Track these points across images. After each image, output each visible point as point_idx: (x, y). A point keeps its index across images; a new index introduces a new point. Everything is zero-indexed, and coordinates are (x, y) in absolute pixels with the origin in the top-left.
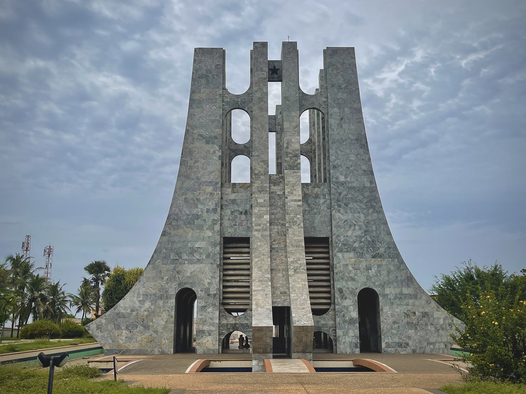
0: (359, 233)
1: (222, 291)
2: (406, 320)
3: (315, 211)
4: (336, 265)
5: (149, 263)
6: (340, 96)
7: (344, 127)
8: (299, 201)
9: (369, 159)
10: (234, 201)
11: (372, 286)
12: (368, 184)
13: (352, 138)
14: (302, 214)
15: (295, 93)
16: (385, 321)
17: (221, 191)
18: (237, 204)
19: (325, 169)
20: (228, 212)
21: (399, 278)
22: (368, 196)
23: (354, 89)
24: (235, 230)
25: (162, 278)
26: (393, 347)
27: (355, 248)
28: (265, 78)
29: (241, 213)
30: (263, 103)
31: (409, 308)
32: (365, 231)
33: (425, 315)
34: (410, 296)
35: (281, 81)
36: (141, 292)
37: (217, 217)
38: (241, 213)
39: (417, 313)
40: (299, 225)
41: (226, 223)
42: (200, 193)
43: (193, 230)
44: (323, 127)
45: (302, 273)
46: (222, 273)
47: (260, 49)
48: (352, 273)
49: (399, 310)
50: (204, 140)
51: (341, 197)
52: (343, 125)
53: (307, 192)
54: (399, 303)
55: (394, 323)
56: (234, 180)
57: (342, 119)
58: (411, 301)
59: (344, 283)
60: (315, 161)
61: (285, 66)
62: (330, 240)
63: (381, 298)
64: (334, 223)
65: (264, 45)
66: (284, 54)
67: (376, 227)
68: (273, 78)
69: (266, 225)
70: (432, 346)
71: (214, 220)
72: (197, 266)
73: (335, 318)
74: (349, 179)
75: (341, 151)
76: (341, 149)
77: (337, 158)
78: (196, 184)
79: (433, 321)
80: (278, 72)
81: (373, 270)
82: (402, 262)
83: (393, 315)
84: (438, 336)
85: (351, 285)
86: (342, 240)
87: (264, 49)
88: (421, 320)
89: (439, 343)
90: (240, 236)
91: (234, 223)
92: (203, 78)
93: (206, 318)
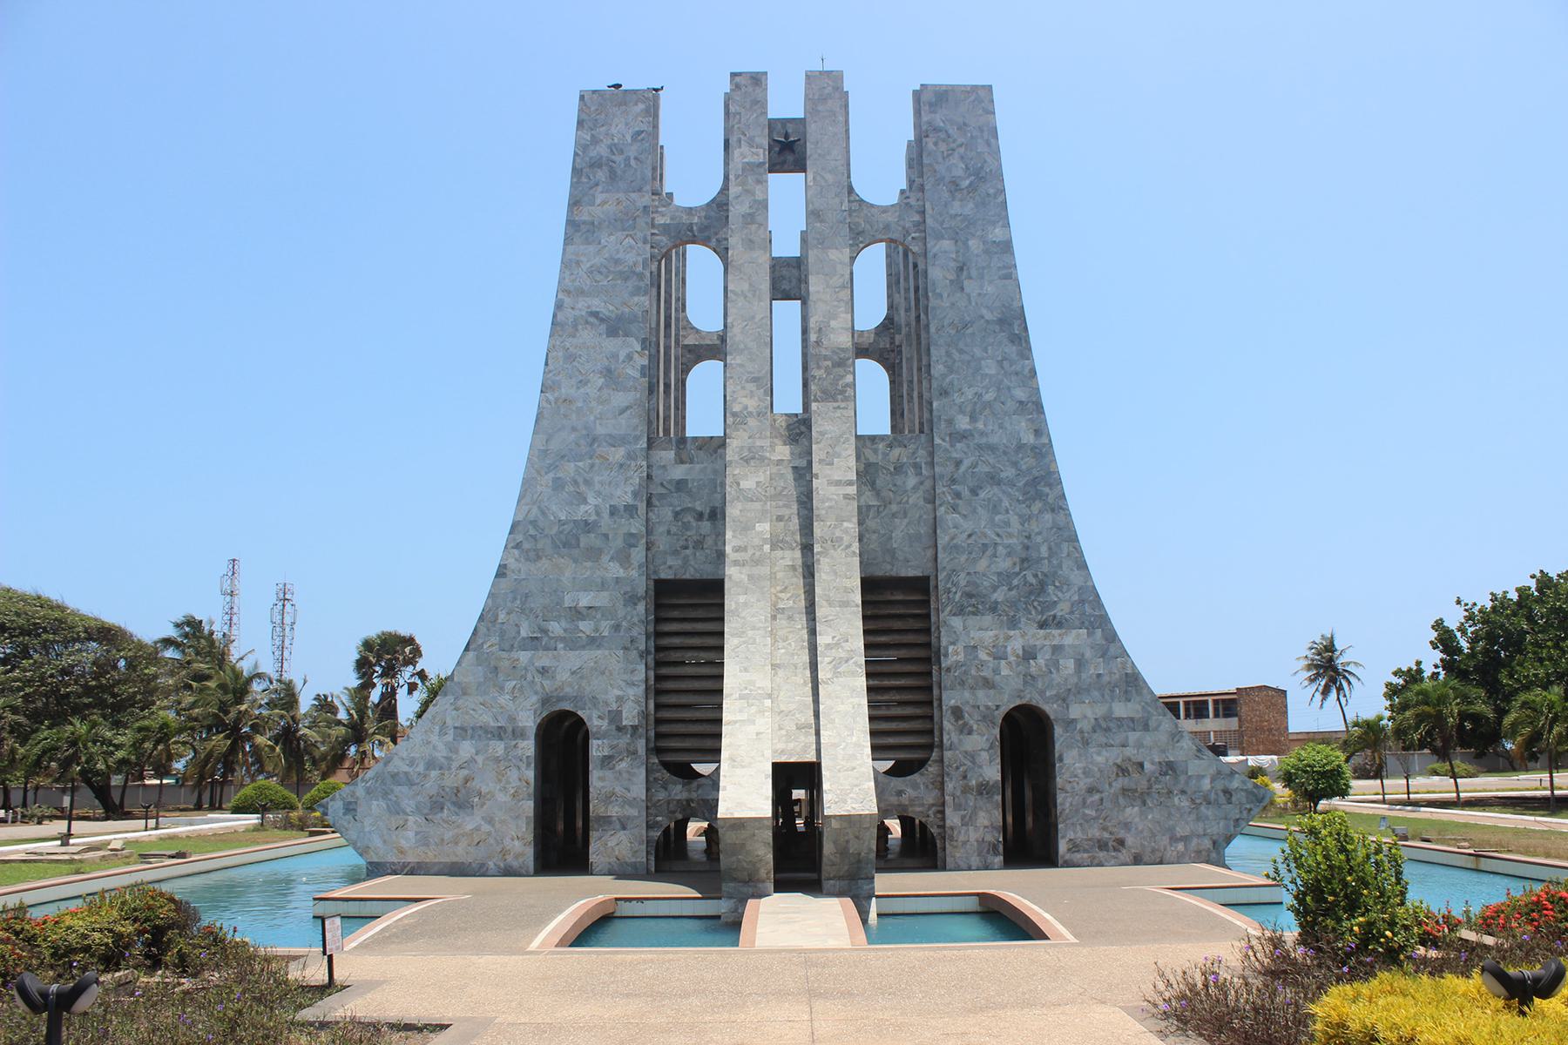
0: (1004, 564)
1: (652, 718)
2: (1118, 785)
3: (894, 508)
4: (946, 648)
5: (467, 649)
6: (956, 207)
7: (967, 290)
8: (850, 483)
9: (1033, 373)
10: (680, 485)
11: (1031, 697)
12: (1029, 438)
13: (988, 316)
14: (855, 520)
15: (837, 200)
16: (1068, 787)
17: (647, 458)
18: (689, 493)
19: (921, 396)
20: (667, 513)
21: (1106, 679)
22: (1029, 469)
23: (991, 191)
24: (686, 560)
25: (502, 688)
26: (1086, 851)
27: (996, 602)
28: (761, 165)
29: (700, 516)
30: (754, 227)
31: (1130, 752)
32: (1023, 561)
33: (1169, 768)
34: (1131, 723)
35: (804, 171)
36: (449, 722)
37: (637, 526)
38: (700, 516)
39: (1147, 765)
40: (849, 546)
41: (662, 543)
42: (592, 466)
43: (576, 561)
44: (917, 289)
45: (853, 674)
46: (652, 674)
47: (747, 88)
48: (985, 662)
49: (1103, 758)
50: (603, 327)
51: (963, 468)
52: (966, 283)
53: (872, 459)
54: (1104, 740)
55: (1091, 790)
56: (690, 432)
57: (961, 269)
58: (1133, 737)
59: (967, 694)
60: (900, 375)
61: (812, 130)
62: (932, 583)
63: (1058, 731)
64: (943, 540)
65: (758, 79)
66: (811, 101)
67: (1050, 549)
68: (784, 162)
69: (761, 548)
70: (1181, 846)
71: (632, 535)
72: (588, 656)
73: (942, 783)
74: (980, 425)
75: (961, 352)
76: (961, 345)
77: (951, 370)
78: (582, 442)
79: (1187, 783)
80: (797, 147)
81: (1041, 661)
82: (1112, 637)
83: (1086, 773)
84: (1198, 819)
85: (984, 698)
86: (962, 583)
87: (758, 90)
88: (1157, 781)
89: (1199, 836)
90: (698, 576)
91: (681, 543)
92: (600, 166)
93: (618, 785)
